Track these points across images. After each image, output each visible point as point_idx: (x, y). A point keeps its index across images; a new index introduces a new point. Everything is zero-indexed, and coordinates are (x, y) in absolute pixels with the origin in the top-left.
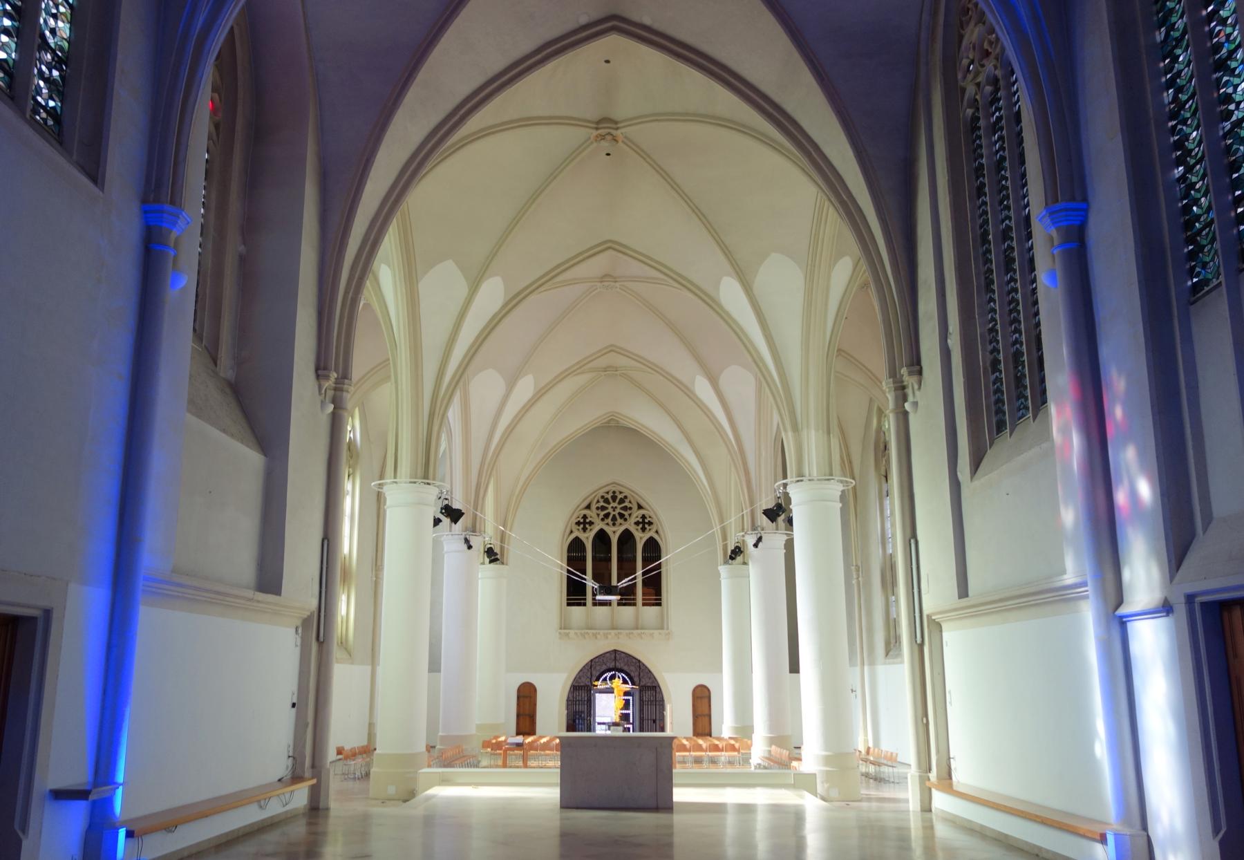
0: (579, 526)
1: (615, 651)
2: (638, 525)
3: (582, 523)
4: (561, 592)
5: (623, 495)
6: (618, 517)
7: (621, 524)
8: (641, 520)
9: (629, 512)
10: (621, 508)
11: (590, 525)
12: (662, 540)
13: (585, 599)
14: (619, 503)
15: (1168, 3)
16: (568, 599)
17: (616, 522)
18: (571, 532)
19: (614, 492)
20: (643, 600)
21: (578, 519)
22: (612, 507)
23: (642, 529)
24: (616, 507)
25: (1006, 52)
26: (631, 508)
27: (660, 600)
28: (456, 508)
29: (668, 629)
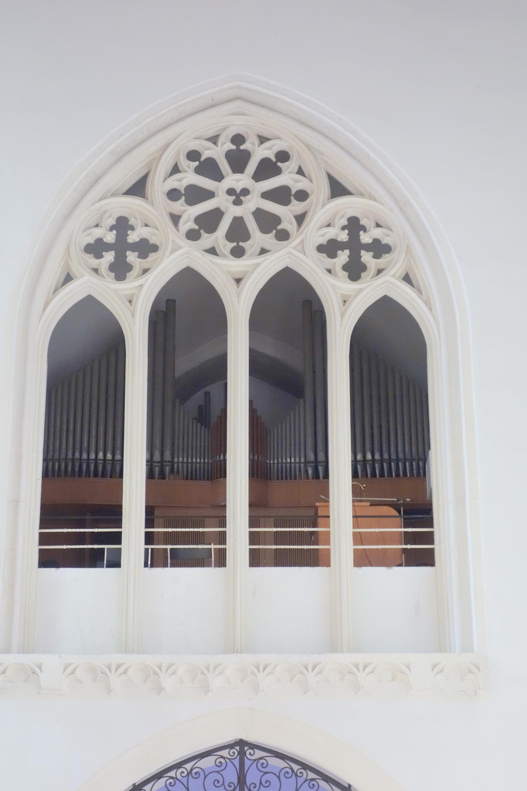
0: (130, 268)
1: (241, 743)
2: (99, 256)
3: (108, 247)
4: (15, 502)
5: (276, 146)
6: (252, 225)
7: (263, 251)
8: (344, 236)
9: (297, 207)
10: (267, 195)
11: (143, 255)
12: (428, 303)
13: (117, 538)
14: (258, 176)
15: (157, 468)
16: (44, 539)
17: (204, 235)
18: (68, 278)
19: (238, 139)
20: (358, 539)
21: (98, 233)
22: (231, 192)
23: (112, 268)
24: (245, 192)
25: (387, 255)
26: (302, 195)
27: (429, 538)
28: (345, 272)
29: (468, 648)
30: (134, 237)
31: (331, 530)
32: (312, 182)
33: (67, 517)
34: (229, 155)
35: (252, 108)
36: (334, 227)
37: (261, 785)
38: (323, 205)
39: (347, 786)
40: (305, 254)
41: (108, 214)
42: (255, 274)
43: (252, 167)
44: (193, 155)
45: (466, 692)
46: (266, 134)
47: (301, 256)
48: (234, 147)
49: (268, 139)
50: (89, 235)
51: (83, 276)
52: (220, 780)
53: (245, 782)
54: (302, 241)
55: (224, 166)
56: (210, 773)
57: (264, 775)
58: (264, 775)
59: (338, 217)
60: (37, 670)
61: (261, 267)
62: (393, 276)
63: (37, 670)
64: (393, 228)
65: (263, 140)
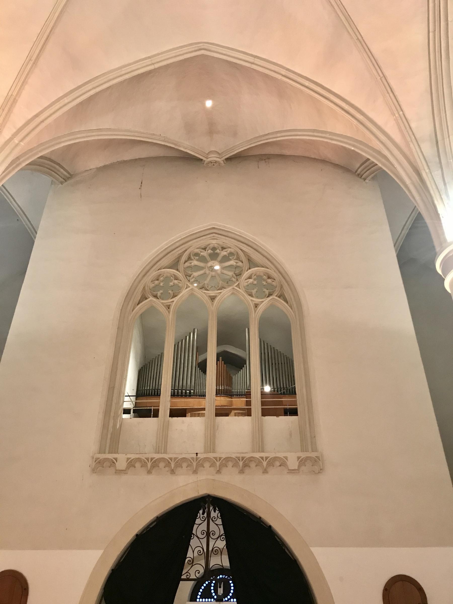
19: (214, 249)
30: (171, 284)
31: (252, 399)
32: (243, 263)
33: (128, 352)
34: (210, 255)
35: (220, 236)
36: (252, 279)
37: (218, 526)
38: (247, 271)
39: (259, 518)
40: (240, 289)
41: (162, 275)
42: (219, 296)
43: (219, 258)
44: (196, 254)
45: (314, 471)
46: (225, 246)
47: (238, 289)
48: (212, 252)
49: (225, 248)
50: (153, 283)
51: (149, 298)
52: (200, 573)
53: (210, 516)
54: (239, 284)
55: (208, 258)
56: (195, 548)
57: (219, 525)
58: (219, 525)
59: (253, 275)
60: (115, 461)
61: (222, 294)
62: (276, 296)
63: (115, 461)
64: (276, 279)
65: (223, 248)
